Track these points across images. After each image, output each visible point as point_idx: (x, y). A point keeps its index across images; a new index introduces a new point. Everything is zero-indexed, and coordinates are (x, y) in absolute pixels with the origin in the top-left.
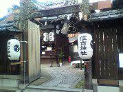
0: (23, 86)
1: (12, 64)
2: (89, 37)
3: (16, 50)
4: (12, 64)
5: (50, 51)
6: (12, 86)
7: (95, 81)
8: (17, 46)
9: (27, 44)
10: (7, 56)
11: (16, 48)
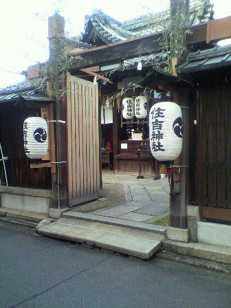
0: (57, 212)
1: (32, 166)
2: (171, 111)
3: (37, 138)
4: (32, 166)
5: (139, 142)
6: (39, 210)
7: (193, 211)
8: (40, 130)
9: (64, 127)
10: (24, 150)
11: (39, 135)
